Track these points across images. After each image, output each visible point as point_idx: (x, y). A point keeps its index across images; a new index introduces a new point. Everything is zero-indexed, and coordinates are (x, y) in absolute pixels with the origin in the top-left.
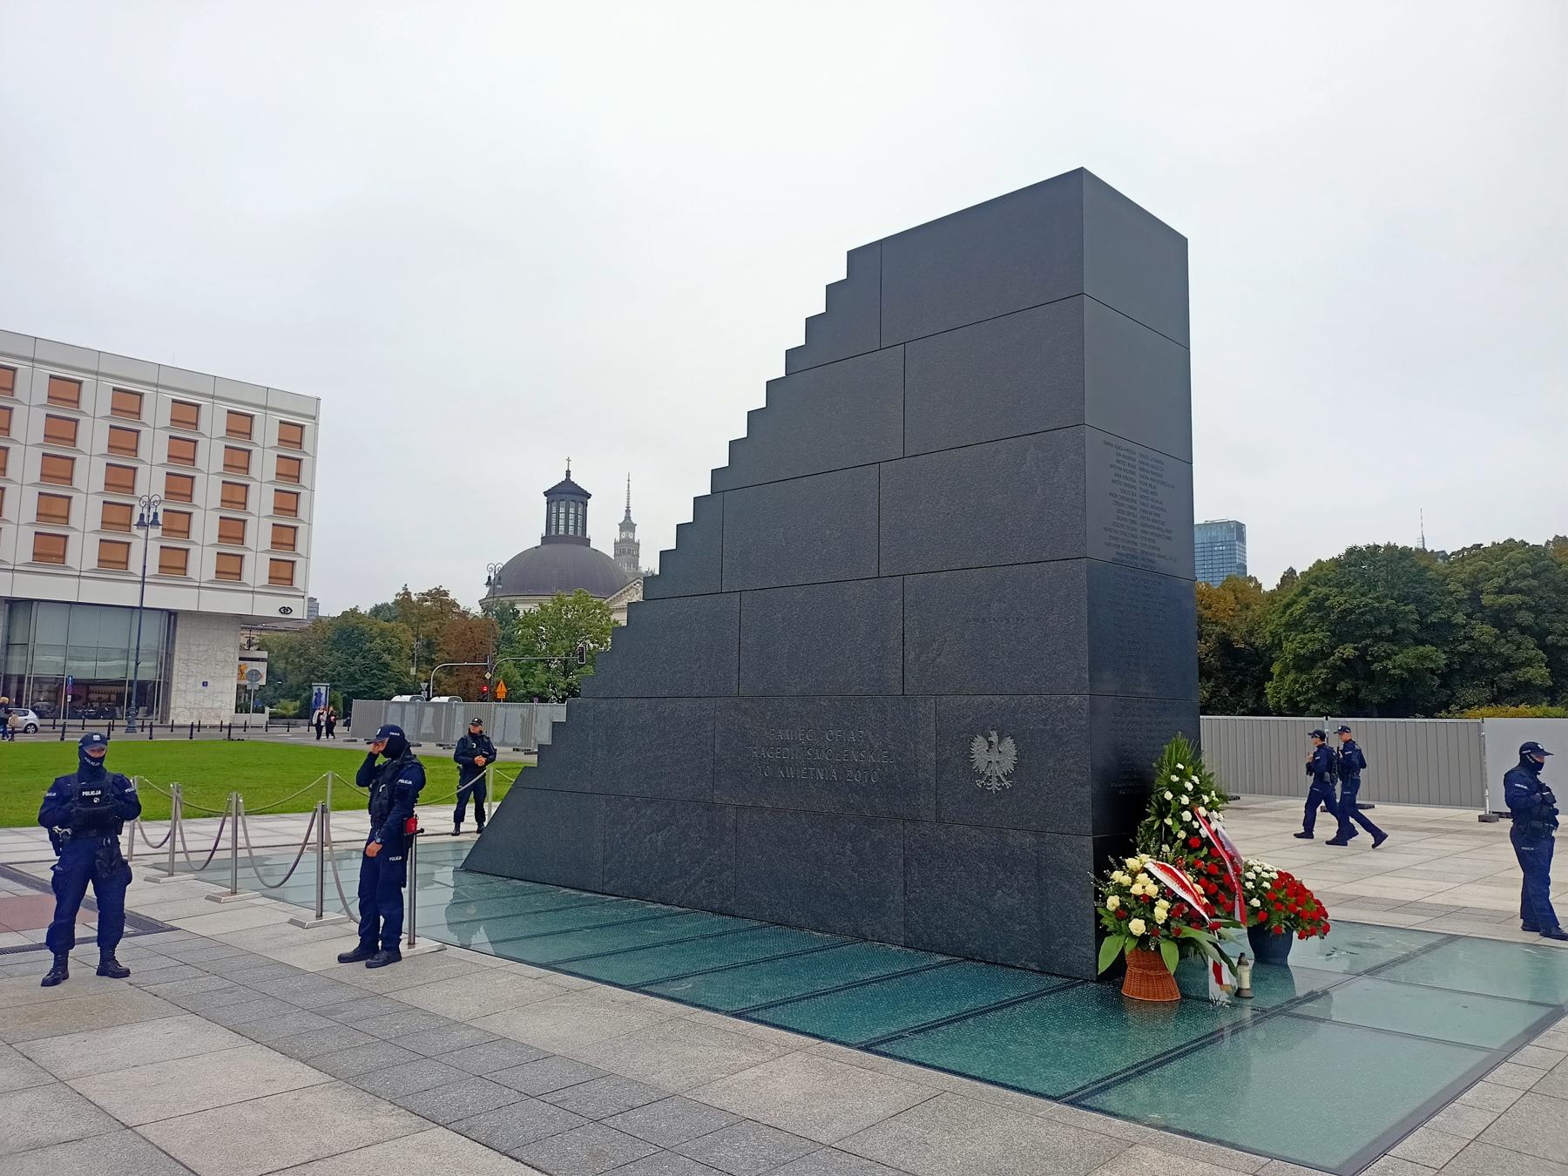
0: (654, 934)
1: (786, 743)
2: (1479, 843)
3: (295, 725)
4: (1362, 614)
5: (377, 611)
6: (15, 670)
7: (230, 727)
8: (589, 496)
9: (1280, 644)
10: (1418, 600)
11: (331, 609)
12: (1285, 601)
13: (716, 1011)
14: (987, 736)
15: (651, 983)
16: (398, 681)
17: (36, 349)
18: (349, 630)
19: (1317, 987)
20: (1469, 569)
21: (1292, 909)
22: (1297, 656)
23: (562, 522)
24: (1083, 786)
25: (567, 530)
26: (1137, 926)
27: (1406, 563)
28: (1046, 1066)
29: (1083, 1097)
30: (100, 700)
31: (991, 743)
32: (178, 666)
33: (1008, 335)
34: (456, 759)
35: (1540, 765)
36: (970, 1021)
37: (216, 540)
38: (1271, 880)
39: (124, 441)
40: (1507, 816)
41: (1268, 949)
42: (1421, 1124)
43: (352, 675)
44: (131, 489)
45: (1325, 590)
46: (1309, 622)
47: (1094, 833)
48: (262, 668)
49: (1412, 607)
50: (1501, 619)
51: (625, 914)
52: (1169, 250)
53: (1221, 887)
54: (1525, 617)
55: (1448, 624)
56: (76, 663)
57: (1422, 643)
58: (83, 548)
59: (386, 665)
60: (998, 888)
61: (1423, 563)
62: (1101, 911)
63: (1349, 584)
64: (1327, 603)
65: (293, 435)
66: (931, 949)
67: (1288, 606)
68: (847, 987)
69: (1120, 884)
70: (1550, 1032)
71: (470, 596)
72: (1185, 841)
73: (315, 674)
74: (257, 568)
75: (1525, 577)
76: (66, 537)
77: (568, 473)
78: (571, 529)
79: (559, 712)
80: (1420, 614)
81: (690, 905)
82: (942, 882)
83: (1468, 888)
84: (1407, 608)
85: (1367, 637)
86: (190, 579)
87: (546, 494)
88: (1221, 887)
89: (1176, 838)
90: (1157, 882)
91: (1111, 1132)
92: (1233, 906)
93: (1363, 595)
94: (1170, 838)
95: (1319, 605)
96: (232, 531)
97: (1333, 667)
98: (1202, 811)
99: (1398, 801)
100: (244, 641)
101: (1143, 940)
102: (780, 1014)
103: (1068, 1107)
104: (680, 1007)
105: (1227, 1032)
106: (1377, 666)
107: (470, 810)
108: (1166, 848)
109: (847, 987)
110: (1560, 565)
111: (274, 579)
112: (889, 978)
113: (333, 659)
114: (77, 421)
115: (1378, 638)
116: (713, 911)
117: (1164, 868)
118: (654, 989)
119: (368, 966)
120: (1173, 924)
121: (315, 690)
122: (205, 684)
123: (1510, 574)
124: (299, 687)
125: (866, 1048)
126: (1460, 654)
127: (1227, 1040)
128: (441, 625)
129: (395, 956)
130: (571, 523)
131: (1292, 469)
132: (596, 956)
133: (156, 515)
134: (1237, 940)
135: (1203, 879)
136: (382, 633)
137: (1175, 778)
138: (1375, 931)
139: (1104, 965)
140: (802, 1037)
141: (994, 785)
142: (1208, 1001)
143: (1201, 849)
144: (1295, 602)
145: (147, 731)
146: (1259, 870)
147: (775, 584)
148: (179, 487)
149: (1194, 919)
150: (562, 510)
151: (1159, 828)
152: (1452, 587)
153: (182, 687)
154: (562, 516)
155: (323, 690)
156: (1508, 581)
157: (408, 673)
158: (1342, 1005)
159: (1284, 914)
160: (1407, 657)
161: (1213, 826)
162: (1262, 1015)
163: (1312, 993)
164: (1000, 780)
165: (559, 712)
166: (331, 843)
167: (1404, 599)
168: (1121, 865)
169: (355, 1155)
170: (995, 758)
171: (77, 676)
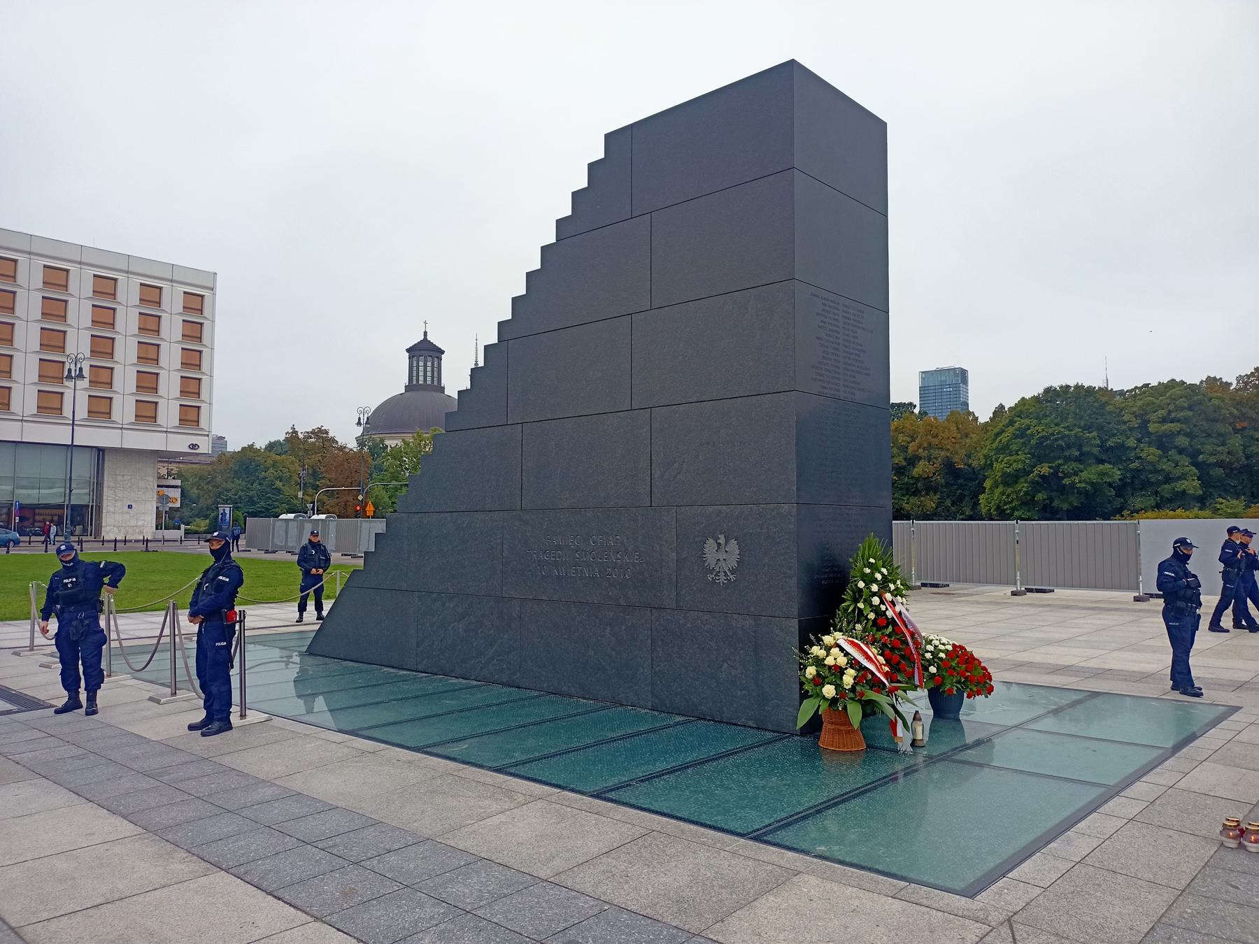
1: (558, 547)
2: (1132, 618)
4: (1056, 440)
5: (271, 446)
8: (443, 352)
10: (1100, 428)
11: (234, 445)
12: (996, 430)
13: (481, 766)
15: (434, 745)
16: (288, 503)
17: (32, 245)
18: (248, 460)
19: (983, 735)
20: (1139, 403)
21: (962, 674)
22: (1004, 475)
23: (421, 374)
26: (829, 691)
28: (743, 808)
29: (765, 834)
32: (107, 492)
33: (746, 195)
34: (299, 562)
35: (1188, 557)
36: (689, 771)
38: (946, 652)
39: (55, 309)
40: (1158, 596)
41: (945, 706)
42: (1038, 850)
43: (251, 498)
44: (62, 348)
45: (1027, 421)
46: (1014, 447)
48: (176, 494)
49: (1095, 434)
50: (1163, 443)
53: (903, 657)
54: (1182, 441)
55: (1122, 447)
56: (23, 491)
57: (1102, 462)
59: (279, 490)
60: (724, 661)
61: (1104, 399)
62: (803, 679)
63: (1045, 416)
65: (195, 304)
67: (997, 435)
70: (1158, 769)
71: (347, 435)
72: (875, 621)
73: (220, 498)
74: (169, 413)
75: (1182, 409)
76: (10, 388)
77: (425, 333)
78: (429, 379)
79: (380, 526)
80: (1100, 438)
81: (485, 679)
83: (1115, 654)
85: (1059, 458)
86: (114, 422)
87: (408, 350)
88: (903, 657)
90: (847, 654)
91: (782, 863)
93: (1057, 425)
95: (1022, 433)
96: (147, 382)
97: (1033, 482)
98: (888, 596)
100: (164, 472)
101: (834, 701)
102: (533, 769)
103: (751, 842)
105: (901, 775)
107: (311, 606)
110: (1210, 400)
112: (632, 736)
114: (14, 293)
115: (1068, 459)
116: (504, 684)
117: (852, 643)
118: (435, 750)
119: (203, 735)
120: (858, 688)
122: (130, 507)
123: (1171, 407)
127: (901, 780)
129: (228, 726)
130: (429, 374)
131: (980, 310)
133: (81, 369)
134: (916, 702)
135: (887, 651)
137: (868, 571)
139: (802, 720)
140: (546, 788)
142: (897, 752)
143: (887, 627)
146: (937, 643)
149: (876, 684)
150: (421, 364)
151: (854, 610)
152: (1125, 418)
153: (111, 509)
154: (421, 369)
155: (227, 511)
156: (1170, 412)
157: (296, 496)
158: (1002, 753)
159: (958, 678)
160: (1090, 473)
161: (898, 609)
162: (930, 760)
165: (380, 526)
166: (180, 635)
167: (1088, 428)
168: (819, 641)
169: (141, 898)
170: (722, 556)
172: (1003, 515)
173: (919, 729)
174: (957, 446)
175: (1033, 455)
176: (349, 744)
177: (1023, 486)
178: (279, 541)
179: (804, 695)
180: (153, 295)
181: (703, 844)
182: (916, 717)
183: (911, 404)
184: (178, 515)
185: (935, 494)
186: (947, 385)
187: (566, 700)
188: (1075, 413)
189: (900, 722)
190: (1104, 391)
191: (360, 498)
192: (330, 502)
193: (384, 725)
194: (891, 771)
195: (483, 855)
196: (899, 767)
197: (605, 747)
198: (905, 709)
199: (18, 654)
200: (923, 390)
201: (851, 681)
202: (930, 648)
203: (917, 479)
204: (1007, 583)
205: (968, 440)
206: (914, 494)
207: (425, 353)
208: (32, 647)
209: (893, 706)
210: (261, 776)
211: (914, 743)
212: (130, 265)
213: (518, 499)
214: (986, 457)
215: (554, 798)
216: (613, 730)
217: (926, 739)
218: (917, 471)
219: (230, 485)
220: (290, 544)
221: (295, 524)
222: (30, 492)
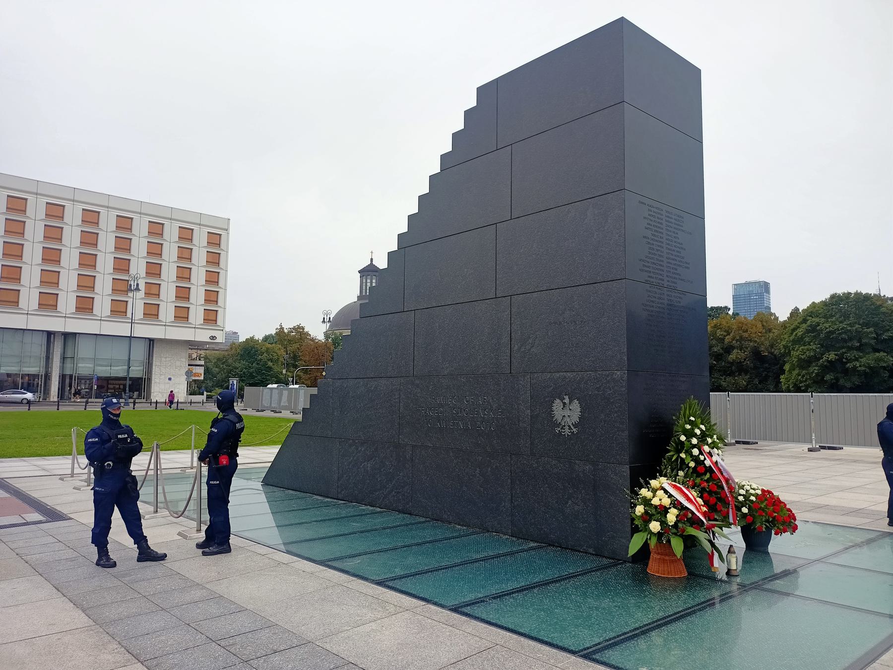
0: (356, 525)
5: (266, 338)
7: (157, 402)
10: (876, 325)
12: (792, 327)
14: (562, 399)
15: (341, 558)
16: (277, 377)
18: (249, 350)
22: (800, 360)
24: (623, 431)
26: (655, 526)
28: (577, 626)
29: (594, 652)
30: (114, 388)
31: (564, 404)
32: (155, 370)
33: (587, 137)
36: (535, 590)
37: (174, 299)
38: (756, 495)
39: (123, 245)
41: (756, 542)
43: (251, 374)
45: (817, 320)
46: (807, 339)
48: (201, 370)
49: (871, 329)
51: (344, 513)
56: (100, 368)
57: (878, 351)
59: (270, 368)
61: (878, 303)
63: (832, 316)
64: (818, 328)
65: (215, 240)
66: (527, 538)
67: (794, 330)
73: (231, 373)
74: (197, 314)
77: (372, 260)
80: (877, 334)
84: (868, 330)
85: (843, 348)
86: (160, 321)
87: (359, 272)
88: (719, 499)
92: (728, 513)
93: (841, 322)
95: (813, 329)
96: (183, 294)
97: (822, 366)
98: (706, 449)
99: (858, 444)
102: (407, 584)
103: (581, 660)
105: (717, 601)
113: (240, 365)
115: (850, 349)
116: (399, 511)
120: (680, 525)
121: (231, 382)
122: (170, 379)
125: (455, 610)
127: (717, 606)
128: (301, 346)
133: (138, 285)
134: (731, 538)
135: (706, 494)
137: (688, 427)
140: (415, 600)
141: (567, 431)
144: (799, 327)
145: (131, 405)
147: (434, 305)
148: (154, 270)
149: (695, 522)
151: (677, 460)
155: (235, 382)
159: (766, 518)
160: (868, 360)
161: (714, 459)
162: (744, 588)
163: (785, 571)
166: (161, 469)
167: (867, 325)
170: (567, 413)
171: (99, 375)
172: (798, 390)
173: (733, 561)
174: (763, 339)
175: (822, 346)
176: (270, 556)
177: (815, 369)
178: (266, 403)
179: (635, 530)
181: (539, 659)
182: (731, 551)
183: (726, 307)
185: (746, 374)
186: (754, 293)
188: (855, 314)
189: (716, 555)
190: (878, 296)
193: (301, 542)
194: (709, 597)
195: (351, 660)
196: (716, 594)
198: (720, 542)
199: (62, 479)
200: (736, 298)
202: (742, 492)
203: (732, 363)
205: (771, 334)
206: (730, 375)
208: (72, 475)
209: (710, 541)
211: (729, 573)
212: (173, 214)
214: (785, 347)
215: (419, 610)
216: (478, 552)
217: (740, 568)
218: (732, 356)
219: (237, 365)
220: (273, 405)
221: (277, 391)
222: (104, 368)
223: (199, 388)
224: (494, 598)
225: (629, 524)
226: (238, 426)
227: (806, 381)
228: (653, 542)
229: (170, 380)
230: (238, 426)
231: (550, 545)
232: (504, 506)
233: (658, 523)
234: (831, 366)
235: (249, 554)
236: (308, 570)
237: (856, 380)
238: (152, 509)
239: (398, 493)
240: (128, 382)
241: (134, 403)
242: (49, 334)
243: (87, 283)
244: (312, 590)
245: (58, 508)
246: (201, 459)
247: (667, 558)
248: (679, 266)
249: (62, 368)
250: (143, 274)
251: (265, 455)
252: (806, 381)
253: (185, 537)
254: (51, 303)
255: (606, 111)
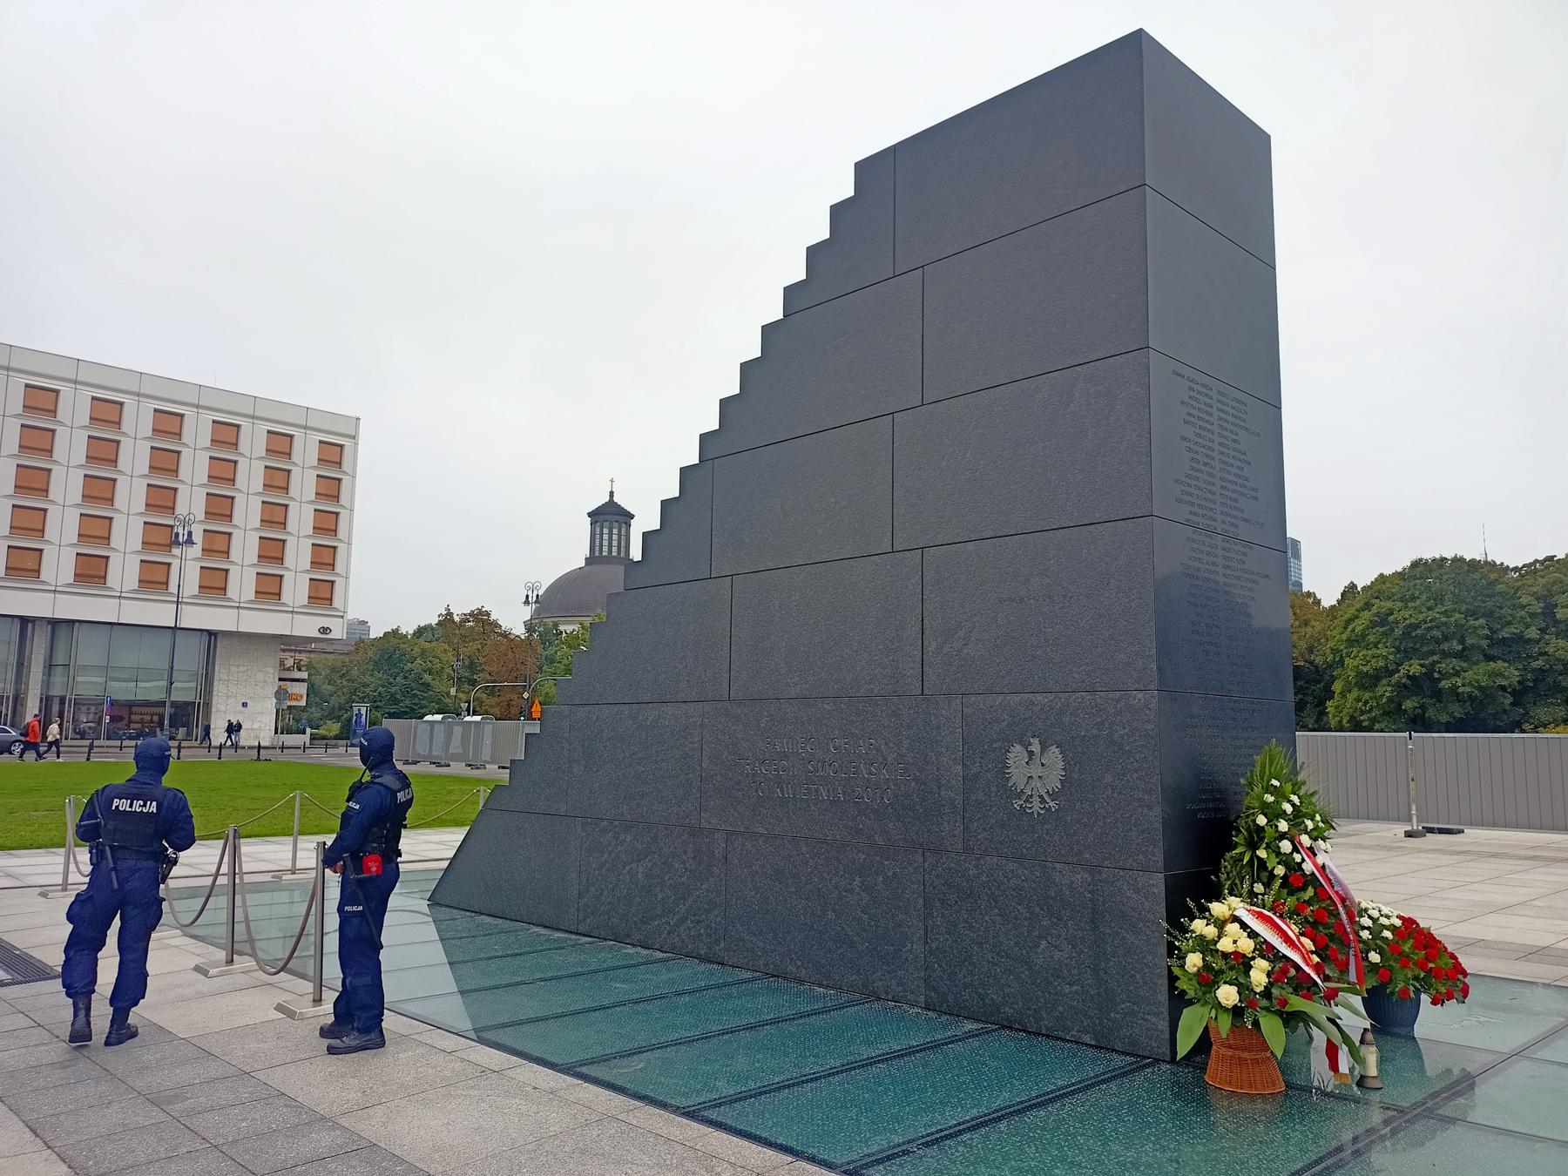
0: (621, 988)
3: (336, 746)
5: (420, 631)
6: (56, 691)
8: (632, 516)
9: (1342, 661)
10: (1489, 614)
12: (1346, 617)
13: (663, 1105)
14: (1026, 745)
15: (592, 1062)
16: (439, 702)
20: (1542, 581)
21: (1422, 965)
22: (1360, 674)
23: (605, 543)
24: (1150, 808)
25: (610, 551)
26: (1227, 994)
27: (1477, 576)
31: (1031, 753)
32: (219, 688)
33: (1056, 262)
36: (1003, 1126)
38: (1393, 928)
39: (165, 462)
41: (1389, 1015)
45: (1389, 604)
46: (1372, 638)
47: (1166, 869)
48: (301, 689)
52: (1244, 149)
53: (1331, 937)
55: (1519, 639)
57: (1493, 658)
58: (124, 569)
59: (427, 685)
60: (1040, 937)
61: (1493, 576)
62: (1177, 971)
63: (1413, 598)
64: (1391, 618)
65: (333, 455)
67: (1349, 621)
68: (847, 1068)
69: (1202, 937)
71: (514, 619)
72: (1285, 878)
73: (354, 696)
74: (296, 589)
76: (107, 558)
77: (612, 494)
78: (614, 549)
82: (971, 928)
84: (1477, 623)
85: (1432, 653)
86: (230, 600)
87: (590, 515)
89: (1272, 876)
90: (1253, 935)
93: (1430, 609)
94: (1264, 875)
96: (272, 551)
98: (1305, 840)
101: (1237, 1012)
104: (618, 1100)
106: (1445, 684)
108: (1259, 888)
109: (847, 1068)
111: (312, 598)
113: (374, 680)
115: (1446, 655)
117: (1260, 916)
120: (1275, 992)
121: (355, 711)
122: (245, 705)
124: (341, 709)
126: (1534, 670)
128: (483, 646)
130: (615, 543)
132: (538, 1020)
133: (190, 534)
136: (423, 652)
137: (1270, 798)
138: (1515, 988)
139: (1182, 1050)
140: (769, 1152)
141: (1036, 806)
143: (1304, 889)
144: (1357, 617)
146: (1375, 914)
148: (220, 508)
149: (1303, 985)
151: (1251, 861)
152: (1524, 601)
154: (606, 537)
157: (448, 694)
159: (1417, 967)
160: (1477, 674)
161: (1320, 859)
164: (1043, 801)
167: (1474, 614)
170: (1037, 772)
172: (1357, 727)
174: (1295, 637)
175: (1398, 650)
177: (1385, 690)
180: (282, 445)
184: (305, 716)
187: (795, 987)
191: (526, 695)
192: (489, 701)
197: (860, 1075)
199: (43, 895)
201: (1264, 980)
204: (1398, 820)
205: (1309, 630)
207: (610, 517)
210: (322, 1109)
212: (256, 408)
213: (725, 684)
214: (1334, 651)
216: (869, 1044)
220: (435, 753)
221: (442, 727)
223: (297, 721)
224: (927, 1145)
225: (1165, 988)
226: (401, 796)
227: (1371, 710)
228: (1225, 1023)
229: (248, 705)
230: (401, 796)
231: (1004, 1027)
232: (911, 951)
233: (1234, 989)
234: (1414, 685)
235: (422, 1050)
236: (544, 1085)
237: (1458, 711)
238: (222, 955)
239: (698, 922)
240: (168, 711)
241: (179, 748)
242: (25, 621)
243: (96, 530)
244: (557, 1128)
245: (36, 954)
246: (329, 858)
247: (1246, 1055)
248: (1241, 494)
249: (47, 684)
250: (201, 516)
251: (424, 847)
252: (1371, 710)
253: (291, 1014)
254: (30, 565)
255: (1109, 202)
